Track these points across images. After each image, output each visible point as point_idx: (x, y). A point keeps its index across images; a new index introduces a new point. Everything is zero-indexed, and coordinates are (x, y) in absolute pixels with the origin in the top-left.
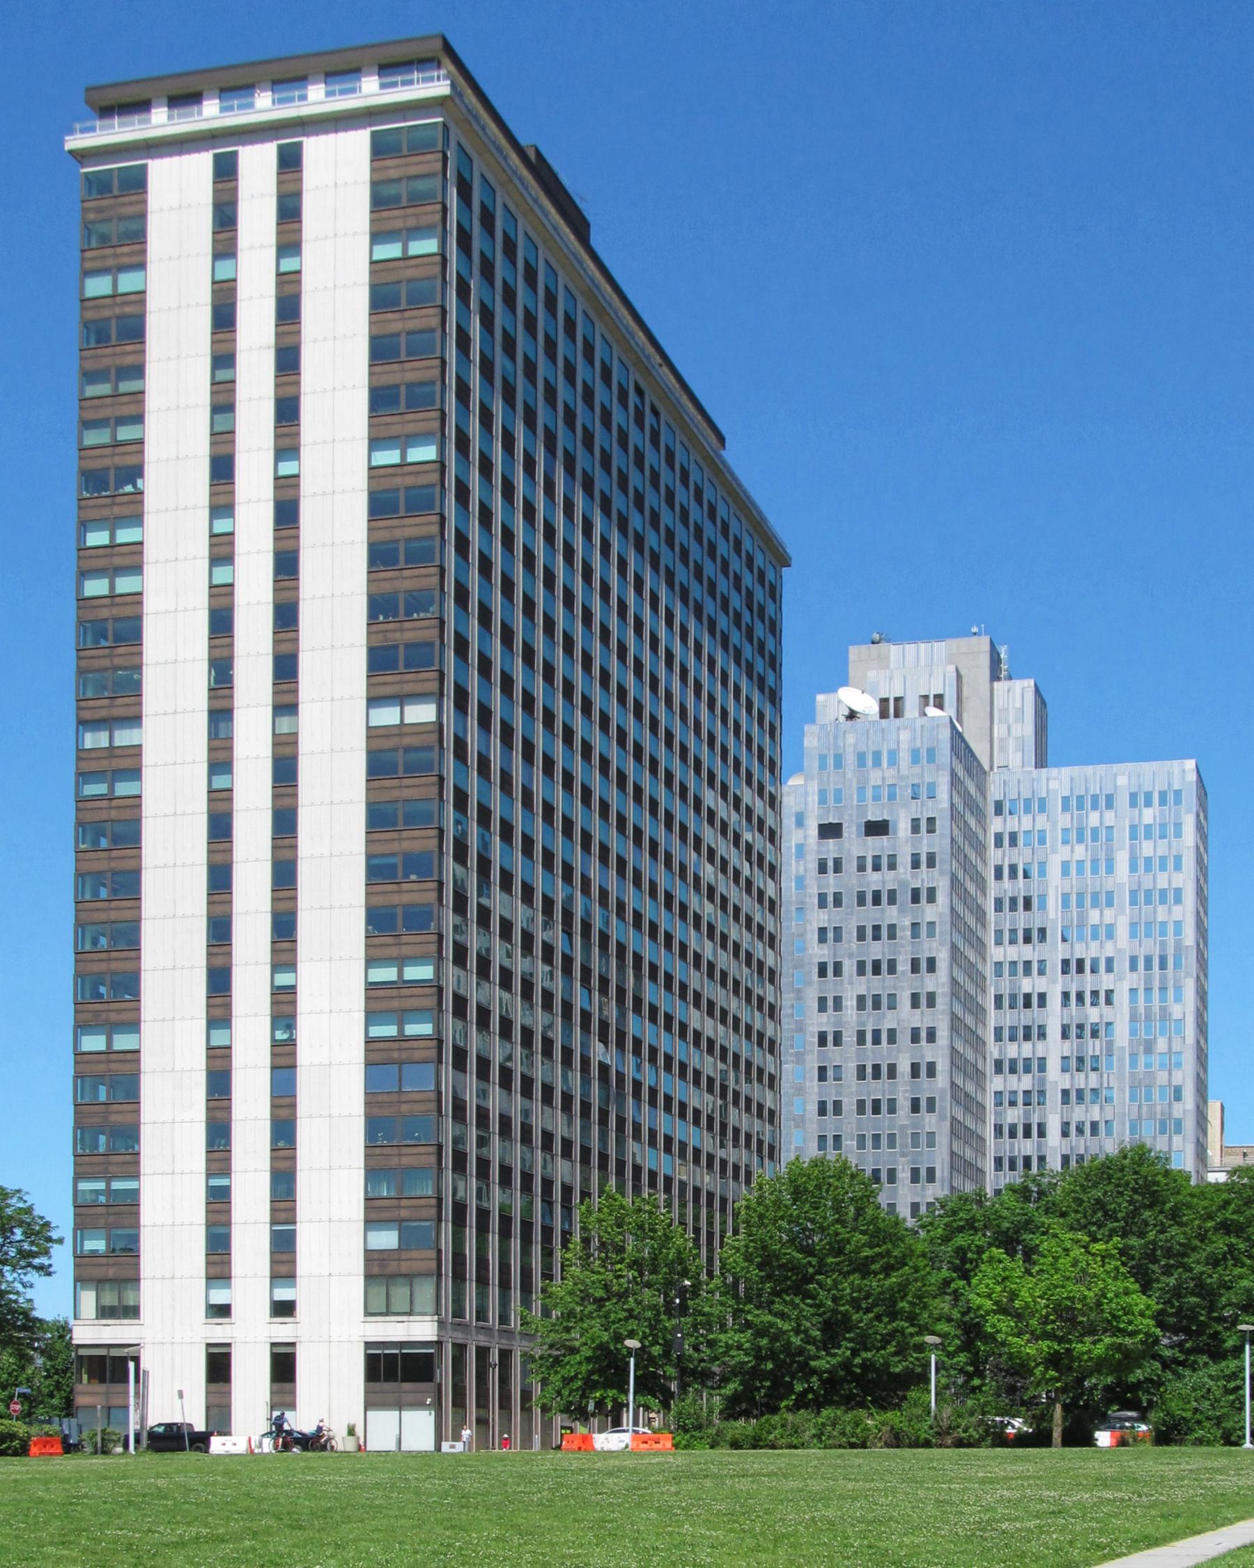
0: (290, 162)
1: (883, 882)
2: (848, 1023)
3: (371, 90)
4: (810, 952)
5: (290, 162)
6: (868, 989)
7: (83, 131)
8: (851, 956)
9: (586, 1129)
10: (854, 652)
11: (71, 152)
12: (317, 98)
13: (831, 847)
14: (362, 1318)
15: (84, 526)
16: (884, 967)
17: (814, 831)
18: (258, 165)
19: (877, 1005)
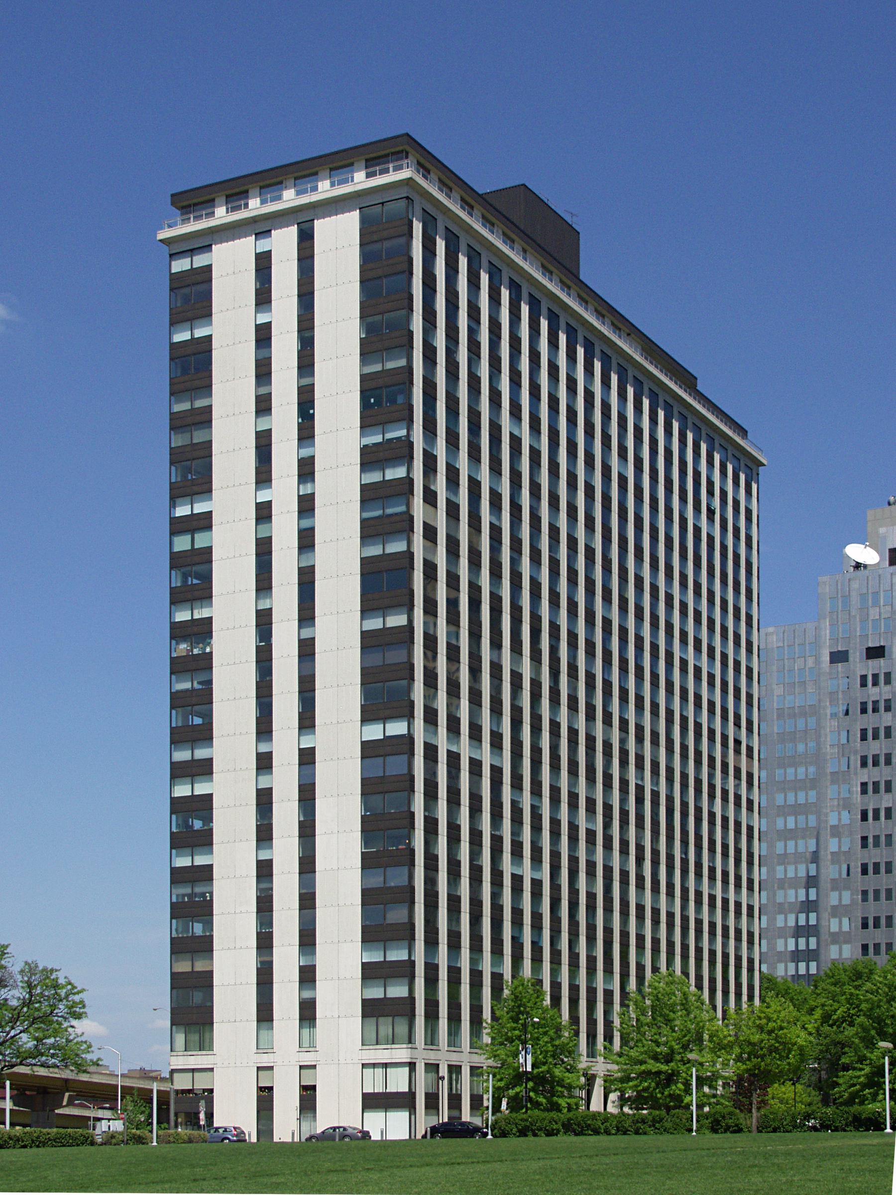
0: (306, 238)
1: (880, 694)
2: (854, 805)
3: (360, 180)
4: (824, 751)
5: (306, 238)
6: (869, 777)
7: (170, 226)
8: (856, 753)
9: (725, 889)
10: (870, 514)
11: (160, 241)
12: (325, 189)
13: (840, 669)
14: (360, 1047)
15: (173, 505)
16: (882, 760)
17: (826, 658)
18: (284, 243)
19: (876, 790)
